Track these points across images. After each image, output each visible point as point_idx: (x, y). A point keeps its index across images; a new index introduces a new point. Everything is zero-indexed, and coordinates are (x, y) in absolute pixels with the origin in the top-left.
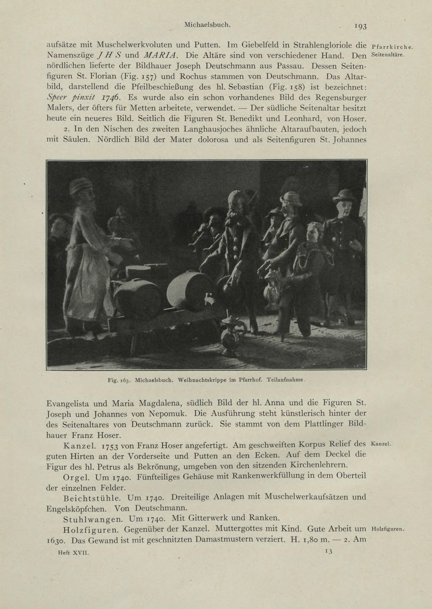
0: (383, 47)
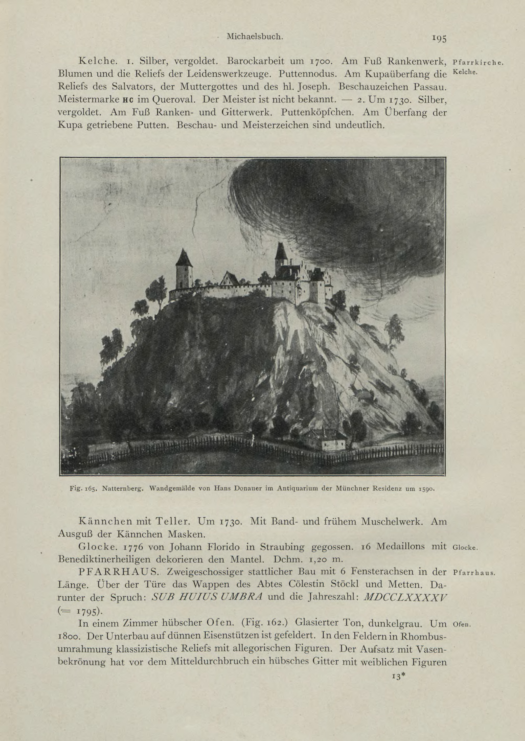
0: (466, 63)
